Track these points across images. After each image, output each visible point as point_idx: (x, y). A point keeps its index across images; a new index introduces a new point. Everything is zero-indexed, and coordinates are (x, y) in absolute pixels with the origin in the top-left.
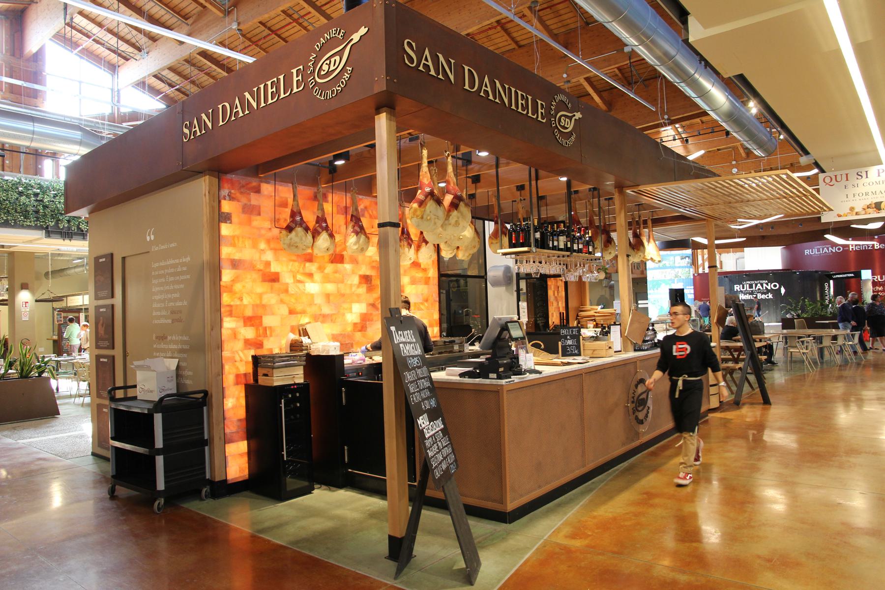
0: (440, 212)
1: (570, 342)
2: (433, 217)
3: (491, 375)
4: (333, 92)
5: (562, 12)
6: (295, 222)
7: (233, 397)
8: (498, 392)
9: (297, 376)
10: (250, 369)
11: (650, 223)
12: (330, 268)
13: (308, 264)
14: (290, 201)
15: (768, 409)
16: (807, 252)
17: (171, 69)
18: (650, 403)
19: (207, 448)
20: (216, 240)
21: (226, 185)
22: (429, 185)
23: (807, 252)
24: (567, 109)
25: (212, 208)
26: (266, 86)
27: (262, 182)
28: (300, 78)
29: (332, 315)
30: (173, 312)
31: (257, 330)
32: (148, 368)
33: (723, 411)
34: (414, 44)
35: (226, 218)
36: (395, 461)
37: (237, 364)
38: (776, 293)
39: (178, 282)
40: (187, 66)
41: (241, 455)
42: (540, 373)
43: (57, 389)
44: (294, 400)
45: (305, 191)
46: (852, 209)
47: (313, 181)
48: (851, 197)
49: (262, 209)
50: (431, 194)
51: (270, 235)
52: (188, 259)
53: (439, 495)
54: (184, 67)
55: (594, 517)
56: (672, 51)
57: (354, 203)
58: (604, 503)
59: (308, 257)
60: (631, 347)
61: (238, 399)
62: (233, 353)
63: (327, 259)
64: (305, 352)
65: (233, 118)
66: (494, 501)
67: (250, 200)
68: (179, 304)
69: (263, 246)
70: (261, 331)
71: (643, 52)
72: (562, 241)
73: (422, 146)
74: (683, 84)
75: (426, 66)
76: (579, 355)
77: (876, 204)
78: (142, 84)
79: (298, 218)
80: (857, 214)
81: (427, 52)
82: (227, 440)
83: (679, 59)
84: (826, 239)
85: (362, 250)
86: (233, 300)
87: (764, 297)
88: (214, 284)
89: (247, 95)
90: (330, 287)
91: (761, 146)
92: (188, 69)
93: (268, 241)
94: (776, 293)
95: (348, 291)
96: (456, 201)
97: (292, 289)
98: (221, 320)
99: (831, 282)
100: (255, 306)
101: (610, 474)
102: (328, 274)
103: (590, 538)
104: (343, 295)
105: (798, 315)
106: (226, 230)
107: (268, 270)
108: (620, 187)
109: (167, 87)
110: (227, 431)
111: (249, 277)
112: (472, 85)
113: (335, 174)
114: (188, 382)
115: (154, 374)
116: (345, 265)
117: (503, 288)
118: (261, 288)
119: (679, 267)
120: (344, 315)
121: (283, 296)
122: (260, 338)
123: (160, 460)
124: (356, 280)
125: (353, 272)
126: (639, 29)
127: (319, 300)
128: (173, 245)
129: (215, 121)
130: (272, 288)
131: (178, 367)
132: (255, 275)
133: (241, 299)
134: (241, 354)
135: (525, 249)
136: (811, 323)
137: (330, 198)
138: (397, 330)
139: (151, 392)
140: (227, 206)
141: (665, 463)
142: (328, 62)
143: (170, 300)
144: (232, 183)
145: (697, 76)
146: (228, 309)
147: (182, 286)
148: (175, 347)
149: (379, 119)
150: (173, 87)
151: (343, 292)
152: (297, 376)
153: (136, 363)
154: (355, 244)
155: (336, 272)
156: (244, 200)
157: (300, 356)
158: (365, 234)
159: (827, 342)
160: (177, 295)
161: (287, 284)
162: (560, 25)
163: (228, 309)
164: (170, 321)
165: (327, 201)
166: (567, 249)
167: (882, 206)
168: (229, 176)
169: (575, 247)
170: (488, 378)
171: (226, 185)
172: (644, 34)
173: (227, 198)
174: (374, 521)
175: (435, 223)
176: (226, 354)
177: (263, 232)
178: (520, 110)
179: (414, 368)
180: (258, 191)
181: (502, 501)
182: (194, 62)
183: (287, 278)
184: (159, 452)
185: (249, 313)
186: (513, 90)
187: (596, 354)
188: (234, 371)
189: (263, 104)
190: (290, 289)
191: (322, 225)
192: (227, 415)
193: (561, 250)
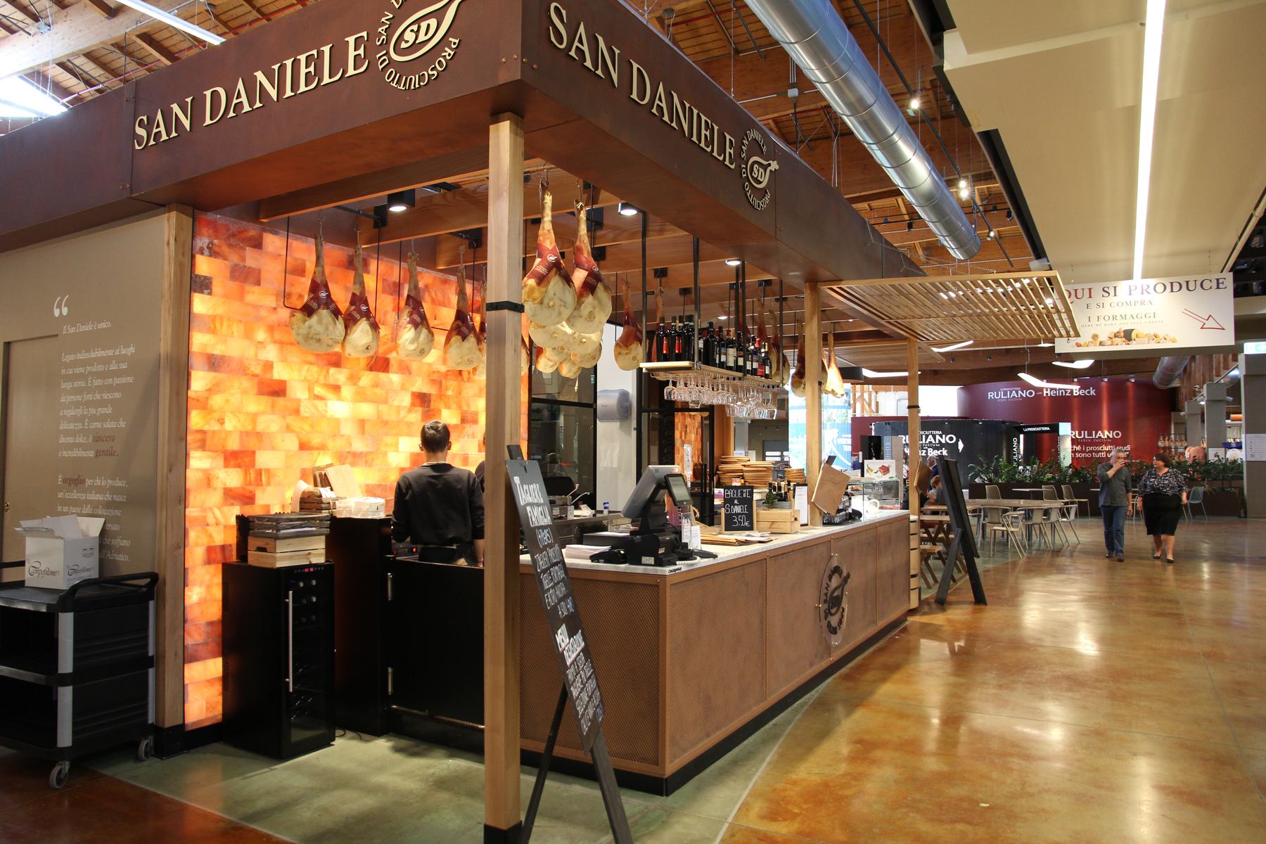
0: (569, 297)
1: (737, 509)
2: (558, 303)
3: (645, 560)
4: (421, 78)
5: (703, 31)
6: (317, 301)
7: (201, 585)
8: (657, 586)
9: (315, 552)
10: (232, 538)
11: (831, 338)
12: (367, 378)
13: (332, 370)
14: (310, 266)
15: (980, 611)
16: (991, 395)
17: (89, 55)
18: (845, 604)
19: (151, 672)
20: (184, 322)
21: (205, 231)
22: (552, 252)
23: (991, 395)
24: (761, 154)
25: (180, 265)
26: (296, 64)
27: (265, 231)
28: (361, 51)
29: (367, 454)
30: (97, 439)
31: (246, 473)
32: (49, 533)
33: (925, 614)
34: (564, 12)
35: (203, 285)
36: (501, 702)
37: (210, 529)
38: (952, 448)
39: (110, 389)
40: (118, 54)
41: (210, 682)
42: (715, 556)
44: (310, 590)
45: (335, 253)
46: (1095, 337)
47: (346, 237)
48: (1094, 319)
49: (263, 275)
50: (556, 266)
51: (273, 318)
52: (132, 349)
53: (582, 756)
54: (113, 56)
55: (795, 783)
56: (869, 98)
57: (413, 279)
58: (801, 758)
59: (334, 358)
60: (818, 519)
61: (209, 587)
62: (204, 510)
63: (363, 363)
64: (325, 513)
65: (231, 114)
66: (643, 760)
67: (243, 259)
68: (109, 425)
69: (261, 335)
70: (253, 476)
71: (828, 91)
72: (730, 356)
73: (544, 189)
74: (874, 147)
75: (580, 52)
76: (751, 528)
77: (1125, 332)
78: (37, 76)
79: (323, 295)
80: (1101, 344)
81: (582, 29)
82: (188, 657)
83: (877, 110)
84: (1020, 379)
85: (422, 352)
86: (208, 423)
88: (178, 393)
89: (260, 76)
90: (367, 410)
91: (961, 245)
92: (120, 60)
93: (271, 329)
94: (952, 448)
95: (393, 417)
96: (592, 281)
97: (306, 409)
98: (186, 455)
99: (1022, 436)
100: (244, 434)
101: (796, 711)
102: (364, 388)
103: (799, 819)
104: (386, 423)
105: (990, 480)
106: (200, 304)
107: (268, 376)
108: (813, 281)
109: (82, 85)
110: (189, 641)
111: (236, 385)
112: (642, 95)
113: (384, 229)
114: (121, 558)
115: (59, 543)
116: (391, 375)
117: (616, 425)
118: (255, 404)
119: (834, 407)
120: (385, 454)
121: (291, 420)
122: (250, 488)
123: (66, 696)
124: (406, 400)
125: (403, 388)
126: (831, 60)
127: (348, 429)
128: (103, 325)
129: (197, 116)
130: (273, 406)
131: (103, 532)
132: (246, 383)
133: (221, 421)
134: (217, 512)
135: (686, 364)
136: (1006, 492)
137: (373, 265)
138: (522, 483)
139: (53, 573)
140: (204, 266)
141: (871, 693)
142: (415, 27)
143: (94, 418)
144: (214, 225)
145: (896, 137)
146: (199, 436)
147: (117, 395)
148: (99, 497)
149: (497, 130)
150: (92, 85)
151: (385, 417)
152: (315, 552)
153: (26, 524)
154: (412, 342)
155: (376, 385)
156: (234, 258)
157: (321, 519)
158: (428, 328)
159: (1038, 518)
160: (108, 410)
161: (299, 401)
162: (698, 49)
163: (199, 436)
164: (91, 454)
165: (368, 272)
166: (738, 368)
167: (1133, 335)
168: (210, 216)
169: (749, 367)
170: (639, 563)
171: (205, 231)
172: (836, 68)
173: (206, 252)
174: (444, 795)
175: (560, 314)
176: (192, 512)
177: (263, 313)
178: (702, 145)
179: (545, 547)
180: (258, 244)
181: (657, 760)
182: (131, 49)
183: (298, 391)
184: (65, 680)
185: (233, 444)
186: (695, 112)
187: (777, 527)
188: (205, 541)
189: (289, 93)
190: (302, 409)
191: (359, 310)
192: (189, 615)
193: (730, 368)
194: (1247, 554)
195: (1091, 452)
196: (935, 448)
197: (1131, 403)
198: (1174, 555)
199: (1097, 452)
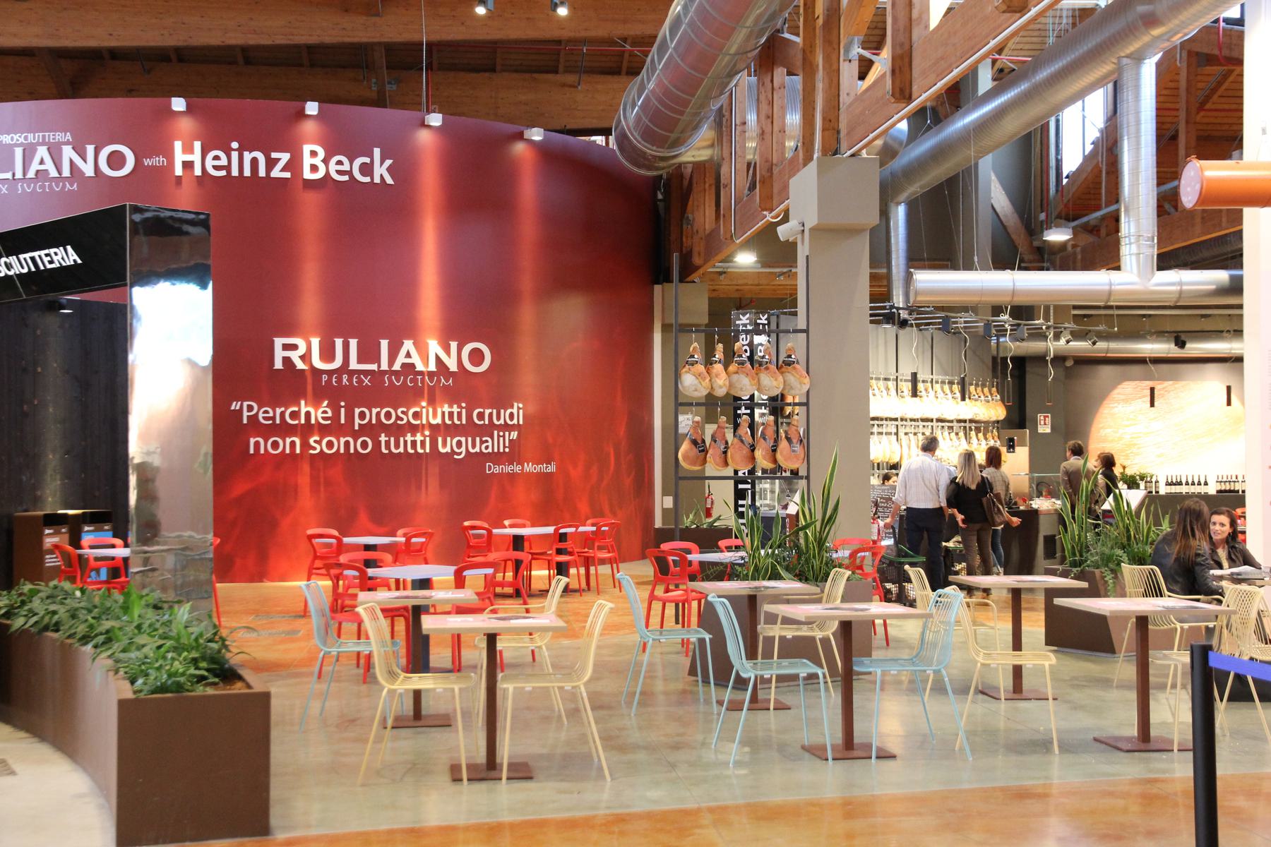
170: (665, 493)
195: (371, 430)
197: (528, 229)
199: (397, 430)
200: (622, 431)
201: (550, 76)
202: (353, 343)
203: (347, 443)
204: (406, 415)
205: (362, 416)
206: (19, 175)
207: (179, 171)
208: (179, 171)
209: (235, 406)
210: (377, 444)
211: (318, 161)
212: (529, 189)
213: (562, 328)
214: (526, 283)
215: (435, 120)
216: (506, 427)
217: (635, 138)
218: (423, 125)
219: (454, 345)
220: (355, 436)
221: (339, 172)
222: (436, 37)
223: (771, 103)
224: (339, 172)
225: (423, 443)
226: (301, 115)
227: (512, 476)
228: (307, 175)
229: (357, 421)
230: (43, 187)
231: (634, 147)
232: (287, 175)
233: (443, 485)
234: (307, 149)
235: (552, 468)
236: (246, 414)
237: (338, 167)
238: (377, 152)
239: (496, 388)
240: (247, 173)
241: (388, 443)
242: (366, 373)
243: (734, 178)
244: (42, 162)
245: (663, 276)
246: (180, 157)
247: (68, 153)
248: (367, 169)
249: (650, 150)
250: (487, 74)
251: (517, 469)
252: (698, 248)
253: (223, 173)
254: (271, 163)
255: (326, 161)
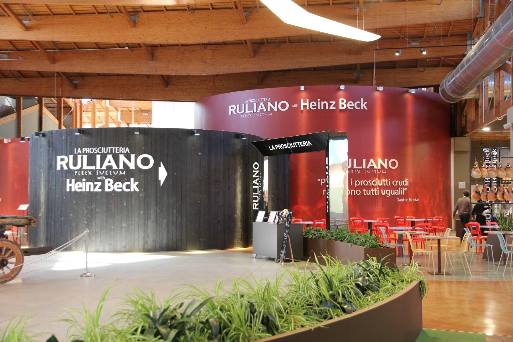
23: (232, 109)
43: (73, 317)
87: (118, 187)
194: (55, 96)
195: (361, 187)
196: (117, 179)
197: (410, 122)
198: (319, 218)
199: (369, 188)
200: (441, 188)
201: (414, 69)
202: (355, 160)
203: (353, 192)
204: (371, 183)
205: (358, 183)
206: (255, 111)
207: (302, 109)
208: (302, 109)
209: (319, 180)
210: (362, 192)
211: (344, 103)
212: (410, 109)
213: (420, 153)
214: (410, 139)
215: (381, 89)
216: (403, 187)
217: (449, 92)
218: (376, 90)
219: (386, 160)
220: (356, 189)
221: (351, 107)
222: (379, 61)
223: (499, 82)
224: (351, 107)
225: (377, 192)
226: (339, 89)
227: (405, 202)
228: (341, 108)
229: (356, 184)
230: (262, 114)
231: (448, 95)
232: (335, 108)
233: (383, 205)
234: (341, 100)
235: (418, 200)
236: (322, 182)
237: (350, 105)
238: (362, 100)
239: (400, 174)
240: (322, 108)
241: (366, 192)
242: (359, 169)
243: (484, 104)
244: (262, 107)
245: (455, 135)
246: (302, 104)
247: (269, 104)
248: (359, 105)
249: (454, 96)
250: (392, 69)
251: (407, 200)
252: (469, 126)
253: (315, 108)
254: (330, 105)
255: (346, 103)
